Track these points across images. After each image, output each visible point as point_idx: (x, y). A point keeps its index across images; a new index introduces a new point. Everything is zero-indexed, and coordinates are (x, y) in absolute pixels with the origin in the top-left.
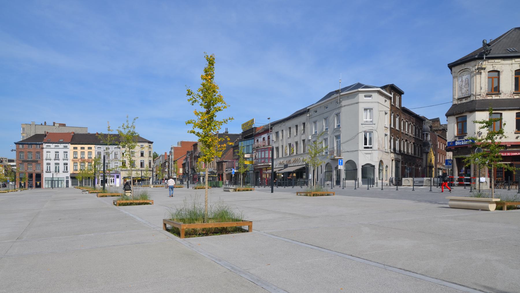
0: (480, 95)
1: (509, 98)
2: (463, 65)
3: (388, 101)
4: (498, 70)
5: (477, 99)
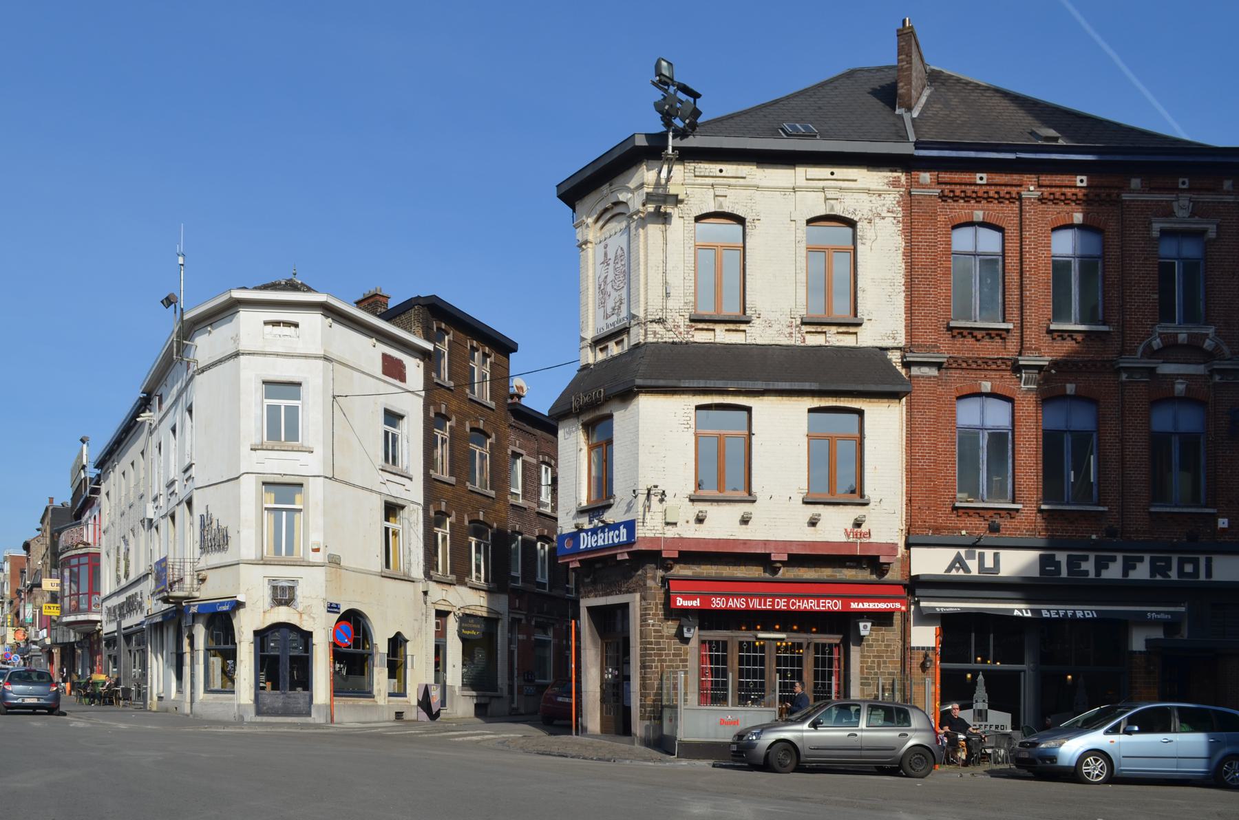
0: (661, 321)
1: (784, 341)
4: (740, 212)
5: (651, 339)
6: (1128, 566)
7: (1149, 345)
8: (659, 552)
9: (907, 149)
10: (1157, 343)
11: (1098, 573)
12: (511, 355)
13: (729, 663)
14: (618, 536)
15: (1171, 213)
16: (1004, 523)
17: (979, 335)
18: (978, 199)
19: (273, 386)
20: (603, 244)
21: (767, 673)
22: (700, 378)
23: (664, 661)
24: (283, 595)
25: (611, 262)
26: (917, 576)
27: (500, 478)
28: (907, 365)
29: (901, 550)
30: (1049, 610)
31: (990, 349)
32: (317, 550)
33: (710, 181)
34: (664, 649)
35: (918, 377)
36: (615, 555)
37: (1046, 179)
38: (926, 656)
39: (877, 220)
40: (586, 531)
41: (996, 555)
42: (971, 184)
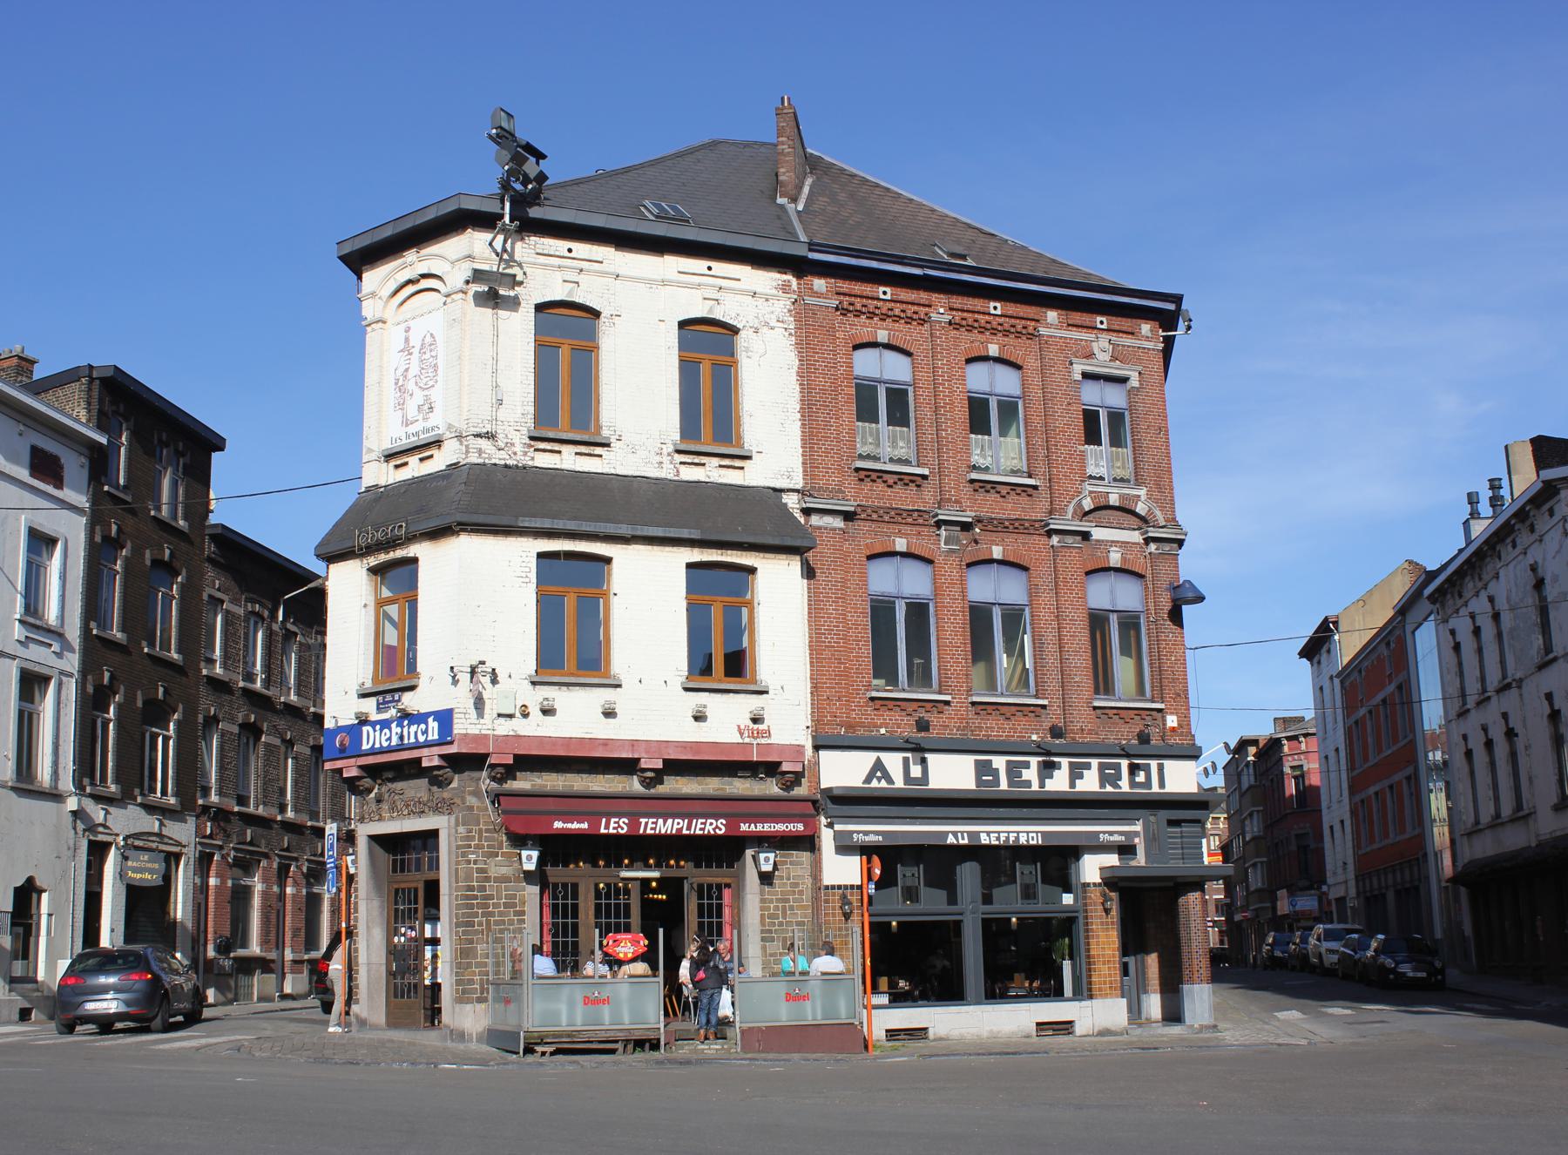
0: (490, 436)
2: (411, 256)
5: (474, 459)
6: (1076, 773)
7: (1079, 504)
9: (802, 251)
11: (1042, 785)
12: (215, 456)
13: (581, 915)
14: (425, 732)
15: (1091, 355)
16: (933, 718)
17: (891, 479)
18: (994, 332)
21: (581, 930)
22: (543, 516)
23: (491, 914)
26: (830, 789)
27: (194, 635)
28: (807, 512)
29: (809, 751)
30: (988, 833)
31: (904, 498)
34: (491, 897)
35: (820, 528)
36: (419, 760)
37: (957, 301)
38: (844, 897)
39: (765, 330)
40: (373, 724)
42: (873, 298)
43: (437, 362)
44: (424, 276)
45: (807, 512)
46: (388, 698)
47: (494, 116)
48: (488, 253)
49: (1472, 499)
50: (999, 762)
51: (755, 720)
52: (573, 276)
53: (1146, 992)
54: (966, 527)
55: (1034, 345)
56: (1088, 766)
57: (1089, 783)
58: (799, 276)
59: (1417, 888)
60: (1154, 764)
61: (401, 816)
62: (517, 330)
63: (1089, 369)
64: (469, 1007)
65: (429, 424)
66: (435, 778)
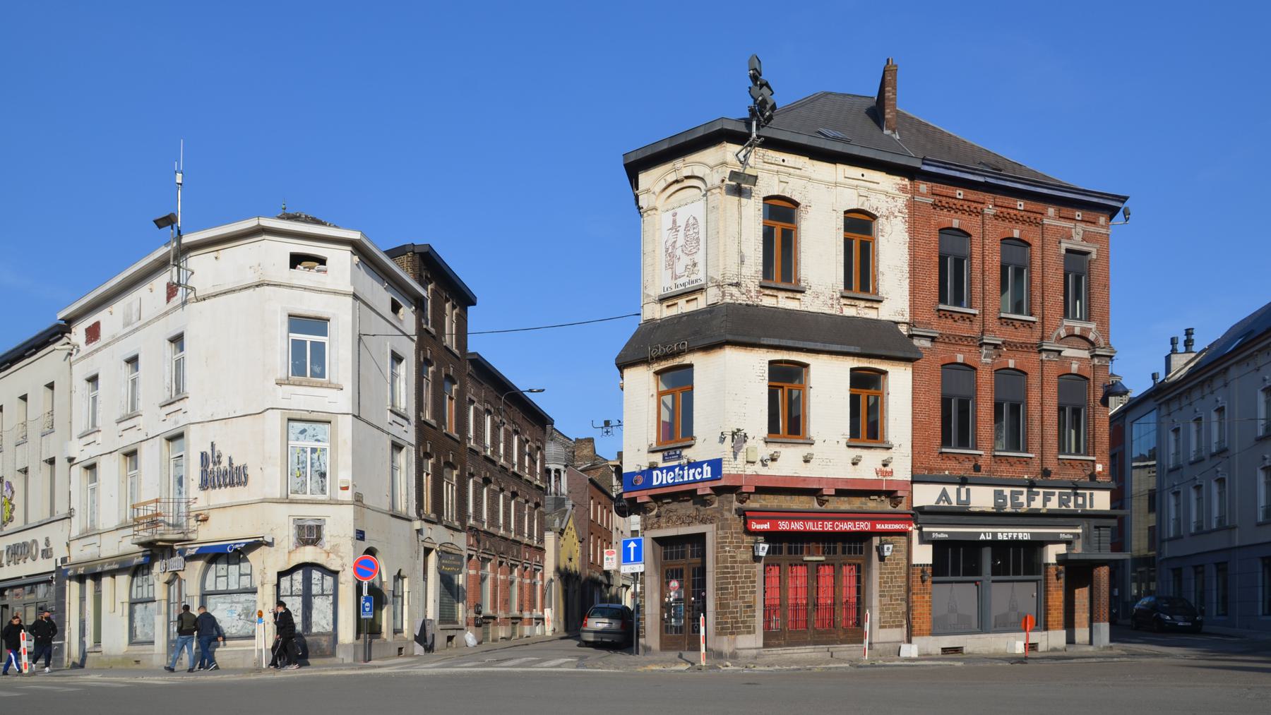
0: (738, 285)
1: (827, 310)
2: (678, 163)
3: (408, 314)
4: (796, 198)
5: (728, 300)
6: (1046, 499)
8: (740, 487)
10: (1063, 333)
12: (470, 309)
14: (702, 473)
18: (957, 210)
19: (298, 322)
20: (671, 212)
22: (774, 337)
24: (310, 534)
25: (682, 229)
32: (347, 488)
33: (775, 168)
37: (1001, 200)
40: (661, 470)
41: (968, 491)
43: (695, 234)
44: (687, 177)
45: (911, 336)
46: (672, 453)
47: (750, 62)
48: (735, 160)
49: (1173, 341)
50: (1007, 491)
51: (885, 465)
52: (784, 178)
53: (1098, 620)
54: (996, 346)
55: (1039, 230)
56: (1053, 494)
57: (1054, 504)
58: (912, 179)
59: (181, 631)
60: (1088, 492)
61: (674, 525)
62: (752, 213)
63: (1070, 246)
64: (725, 638)
65: (693, 277)
66: (702, 501)
